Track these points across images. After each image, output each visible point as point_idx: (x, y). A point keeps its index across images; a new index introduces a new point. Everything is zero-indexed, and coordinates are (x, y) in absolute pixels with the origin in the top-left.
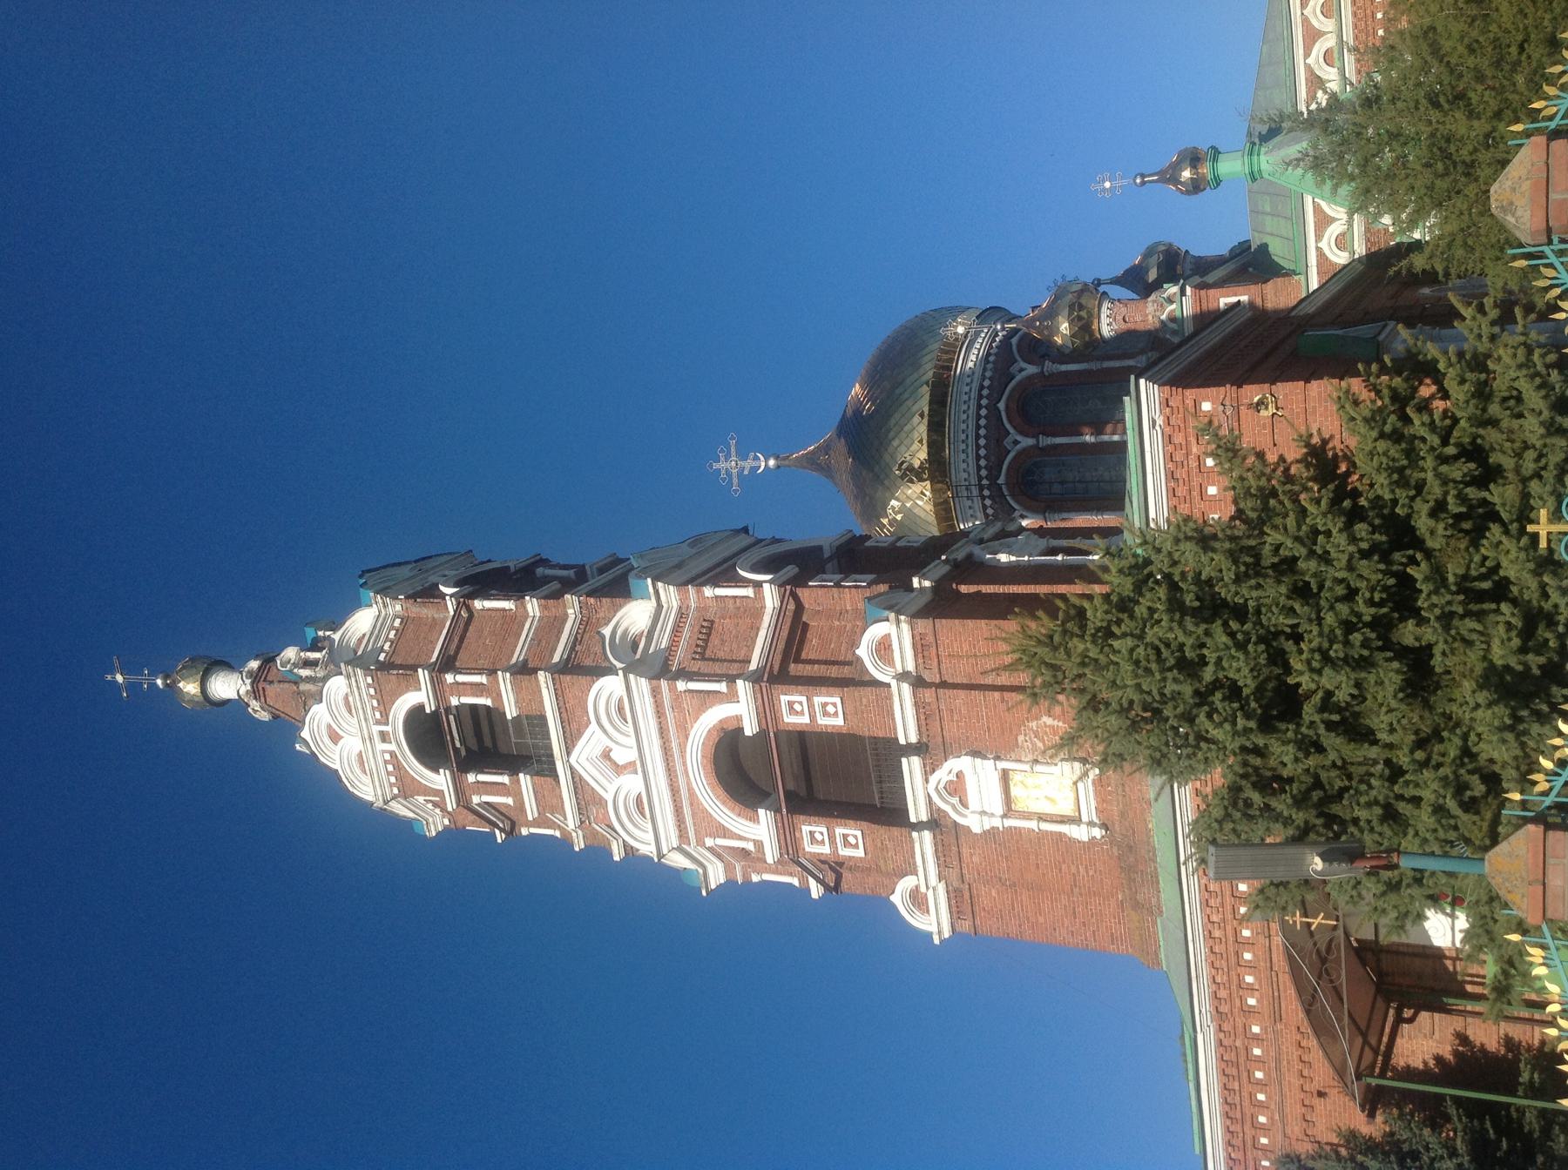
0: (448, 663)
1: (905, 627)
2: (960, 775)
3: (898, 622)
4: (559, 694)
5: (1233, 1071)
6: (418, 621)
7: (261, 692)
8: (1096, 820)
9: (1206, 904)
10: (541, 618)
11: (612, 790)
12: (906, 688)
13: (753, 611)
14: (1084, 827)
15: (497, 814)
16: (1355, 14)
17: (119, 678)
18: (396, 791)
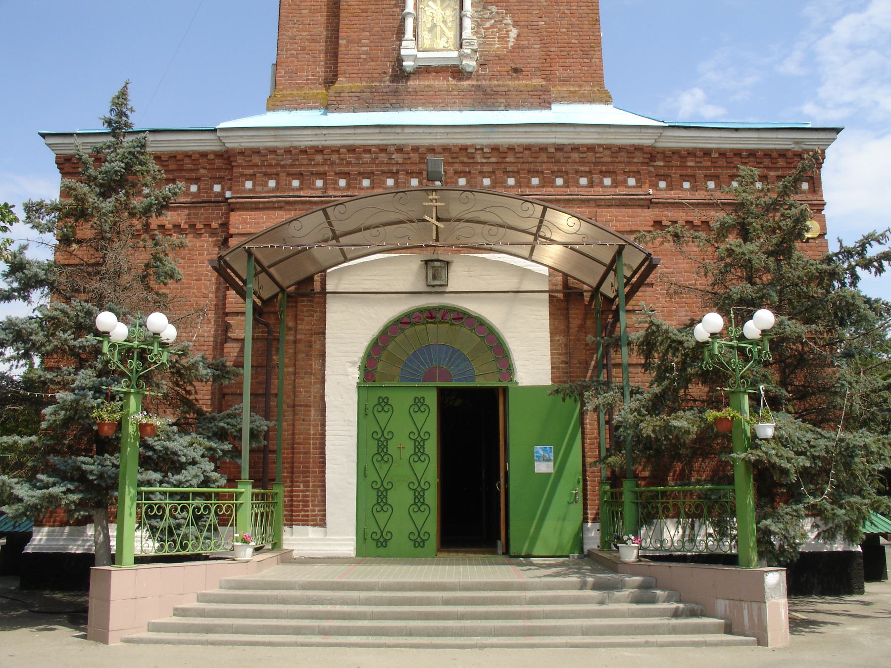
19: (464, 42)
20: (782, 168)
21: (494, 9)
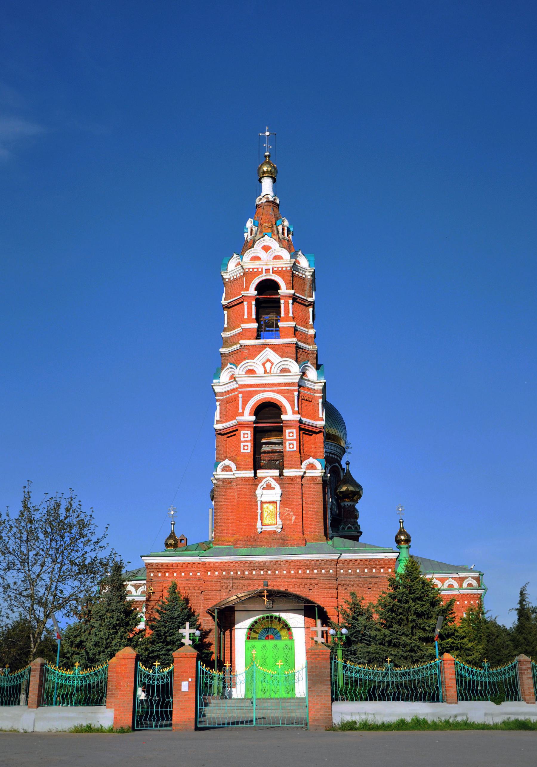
0: (295, 299)
1: (320, 474)
2: (273, 488)
3: (322, 472)
4: (288, 345)
5: (184, 566)
6: (304, 285)
7: (268, 204)
8: (262, 530)
9: (241, 562)
10: (307, 334)
11: (258, 362)
12: (302, 474)
13: (315, 417)
14: (261, 526)
15: (234, 304)
16: (448, 595)
17: (267, 133)
18: (247, 270)
19: (263, 456)
20: (382, 565)
21: (287, 509)
